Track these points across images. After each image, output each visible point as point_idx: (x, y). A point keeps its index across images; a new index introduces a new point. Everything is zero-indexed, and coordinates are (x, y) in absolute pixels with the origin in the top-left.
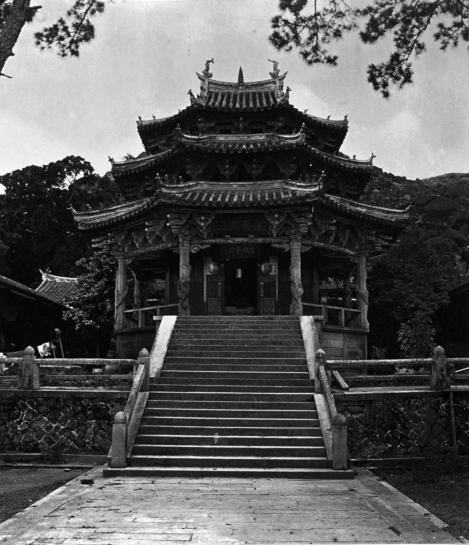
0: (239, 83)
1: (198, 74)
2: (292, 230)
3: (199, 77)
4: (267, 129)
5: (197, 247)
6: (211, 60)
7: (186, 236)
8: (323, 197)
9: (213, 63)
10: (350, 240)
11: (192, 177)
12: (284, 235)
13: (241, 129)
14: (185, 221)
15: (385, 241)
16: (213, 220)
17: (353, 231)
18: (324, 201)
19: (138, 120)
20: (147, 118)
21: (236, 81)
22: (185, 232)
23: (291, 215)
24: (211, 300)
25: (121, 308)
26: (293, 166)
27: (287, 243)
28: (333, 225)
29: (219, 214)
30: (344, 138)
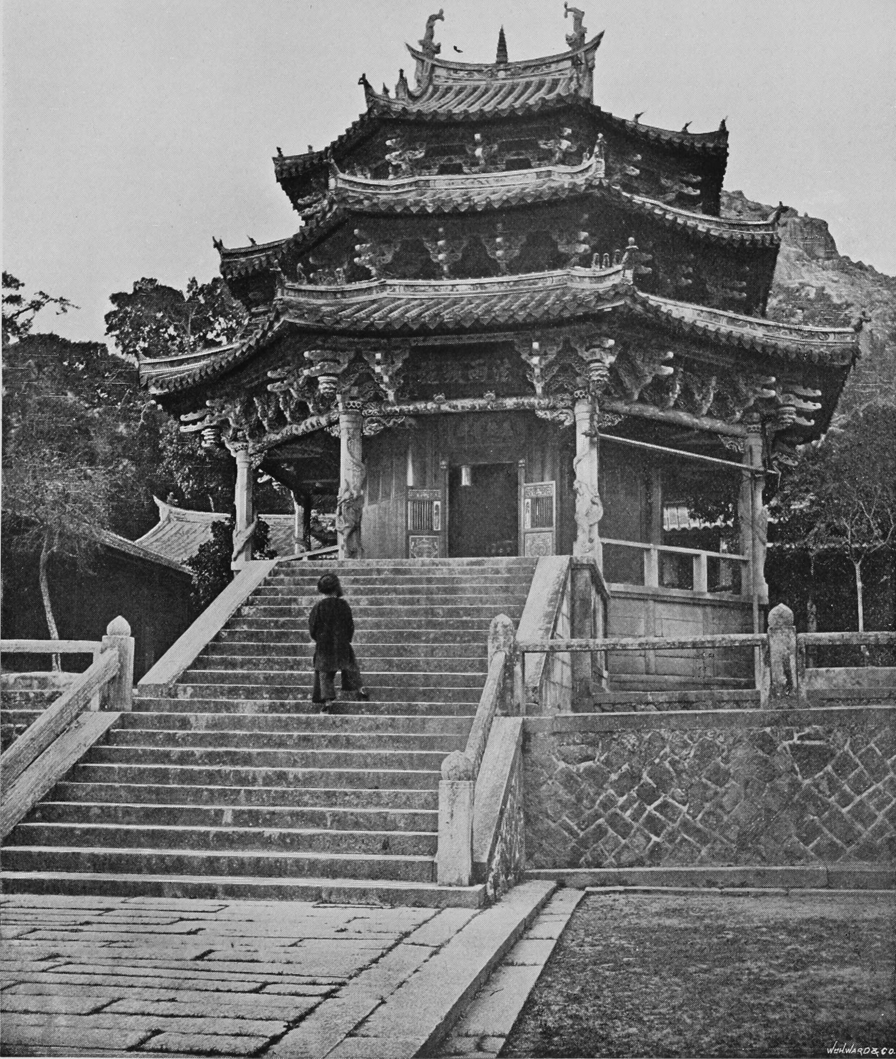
0: (498, 63)
1: (410, 49)
2: (578, 379)
3: (413, 56)
4: (539, 160)
5: (378, 422)
6: (437, 13)
7: (352, 398)
8: (635, 300)
9: (443, 19)
10: (719, 398)
11: (369, 271)
12: (562, 390)
13: (482, 162)
14: (346, 366)
15: (805, 401)
16: (405, 361)
17: (724, 376)
18: (639, 308)
19: (276, 154)
20: (295, 149)
21: (493, 60)
22: (349, 391)
23: (572, 344)
24: (414, 540)
25: (242, 557)
26: (584, 235)
27: (568, 408)
28: (668, 363)
29: (417, 348)
30: (724, 172)
